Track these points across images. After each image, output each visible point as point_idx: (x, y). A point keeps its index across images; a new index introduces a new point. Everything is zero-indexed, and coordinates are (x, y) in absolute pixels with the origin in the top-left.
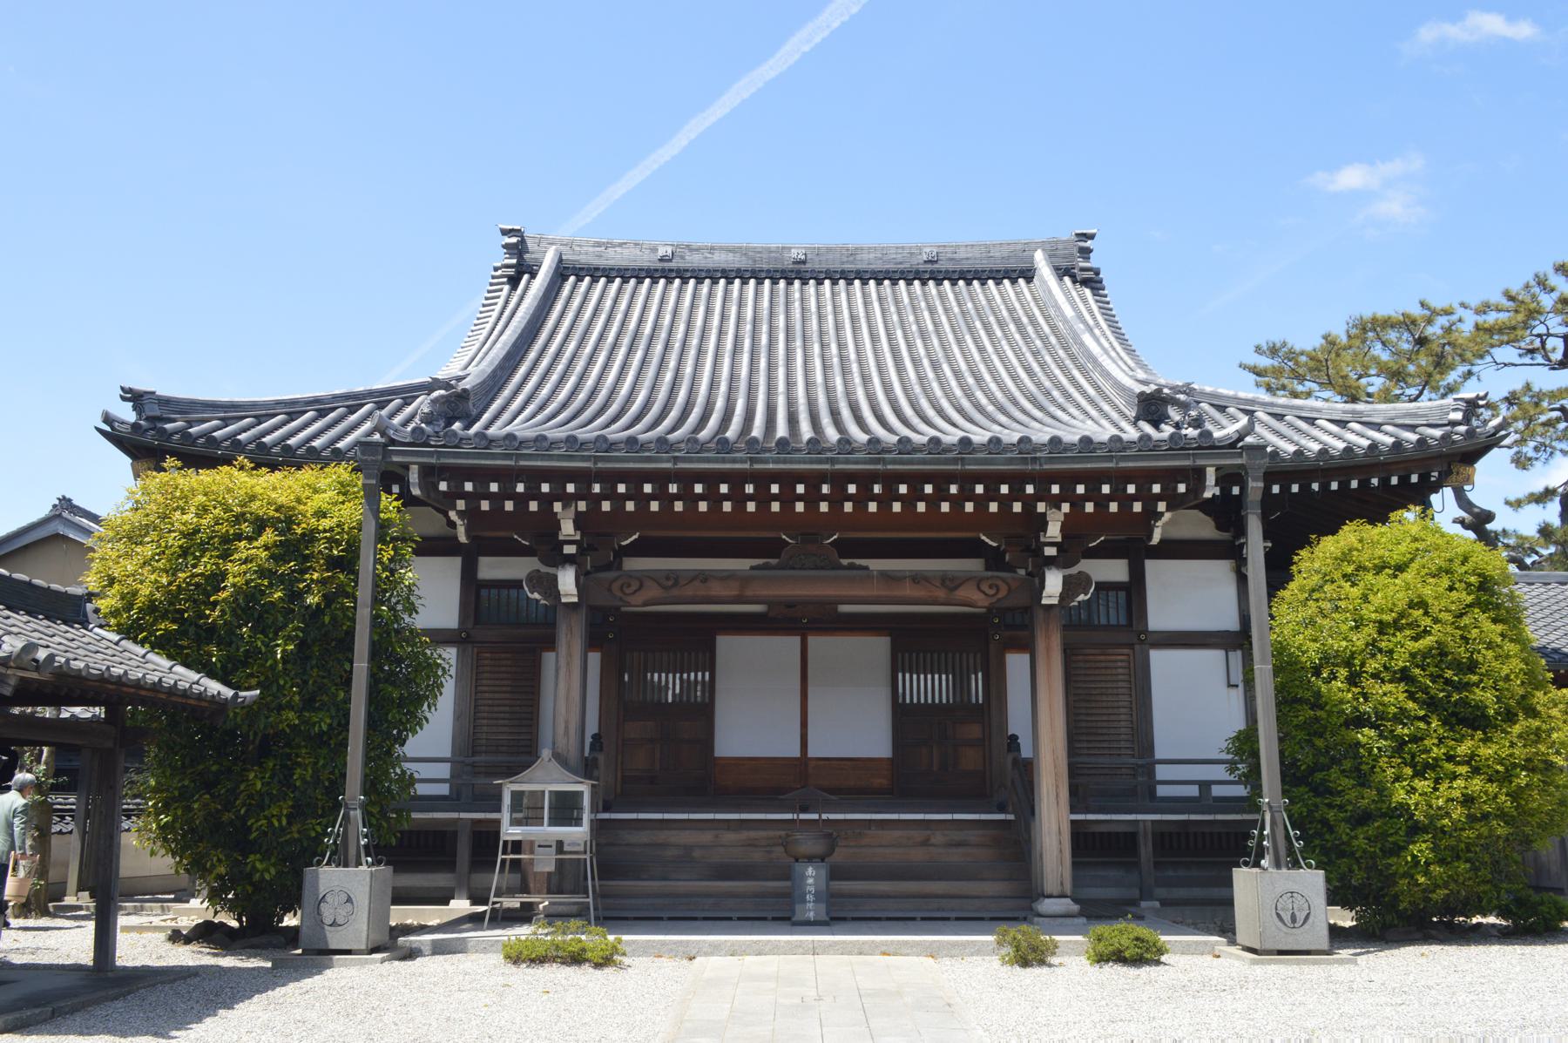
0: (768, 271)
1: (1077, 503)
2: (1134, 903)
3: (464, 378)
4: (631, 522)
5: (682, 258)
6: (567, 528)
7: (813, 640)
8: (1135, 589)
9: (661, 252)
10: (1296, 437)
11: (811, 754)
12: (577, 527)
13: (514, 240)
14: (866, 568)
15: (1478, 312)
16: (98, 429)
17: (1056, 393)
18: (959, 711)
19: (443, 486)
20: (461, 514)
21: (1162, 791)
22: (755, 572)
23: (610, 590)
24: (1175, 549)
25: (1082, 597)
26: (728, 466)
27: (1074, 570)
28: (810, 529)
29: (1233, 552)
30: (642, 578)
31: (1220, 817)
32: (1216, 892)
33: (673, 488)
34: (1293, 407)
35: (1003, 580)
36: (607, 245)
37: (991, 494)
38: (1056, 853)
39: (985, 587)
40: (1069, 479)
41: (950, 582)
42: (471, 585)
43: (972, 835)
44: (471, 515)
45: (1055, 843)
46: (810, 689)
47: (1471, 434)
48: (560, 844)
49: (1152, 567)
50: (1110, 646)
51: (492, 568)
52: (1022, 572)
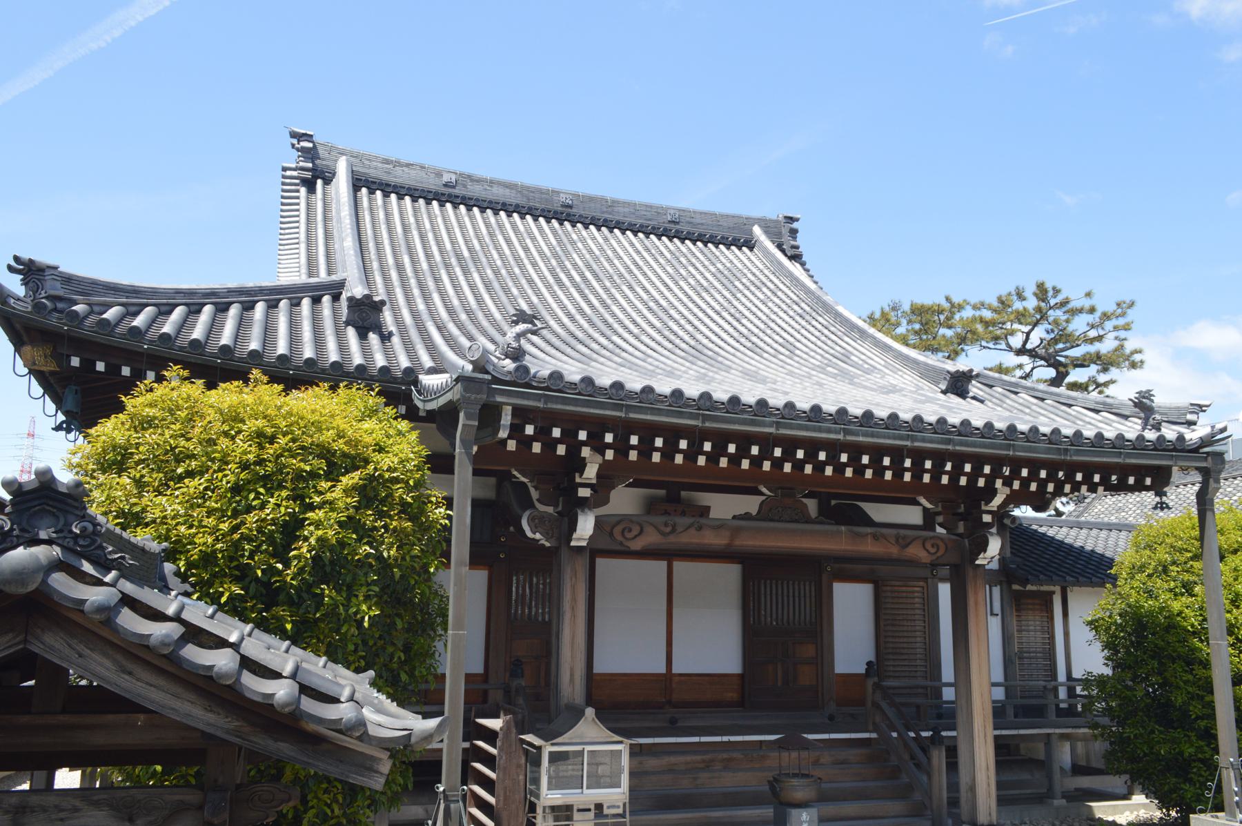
0: (543, 210)
5: (465, 186)
9: (446, 178)
11: (675, 671)
15: (975, 307)
23: (611, 534)
26: (824, 435)
34: (1051, 394)
36: (398, 164)
38: (985, 786)
39: (928, 546)
43: (853, 754)
45: (984, 778)
46: (675, 611)
48: (599, 807)
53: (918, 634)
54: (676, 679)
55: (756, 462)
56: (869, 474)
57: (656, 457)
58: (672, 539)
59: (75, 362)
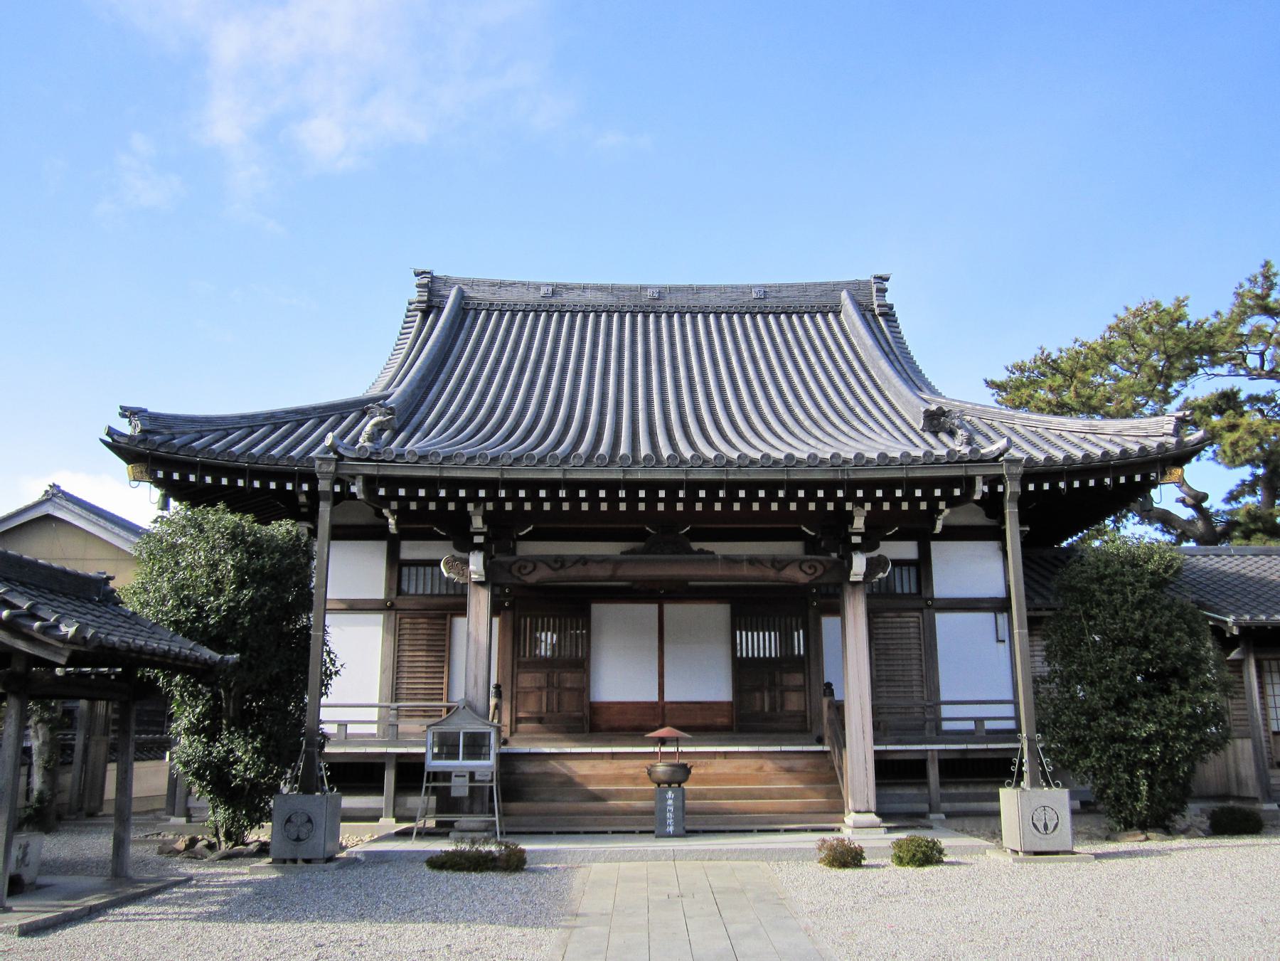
1: (877, 503)
2: (923, 815)
3: (389, 396)
4: (525, 518)
6: (477, 523)
7: (669, 608)
8: (922, 566)
10: (1046, 447)
12: (484, 522)
13: (425, 281)
14: (712, 553)
16: (102, 441)
17: (858, 410)
18: (787, 662)
19: (382, 492)
20: (393, 512)
21: (946, 726)
22: (624, 557)
23: (510, 571)
24: (953, 533)
25: (881, 575)
27: (874, 554)
28: (669, 523)
29: (997, 534)
30: (536, 561)
31: (991, 746)
32: (987, 806)
33: (522, 494)
35: (821, 562)
36: (501, 285)
37: (811, 496)
39: (805, 567)
40: (870, 485)
41: (779, 563)
42: (396, 564)
44: (402, 514)
47: (1179, 443)
48: (472, 775)
49: (935, 546)
50: (905, 608)
51: (410, 551)
52: (834, 555)
53: (914, 662)
54: (668, 707)
55: (802, 503)
56: (547, 506)
57: (642, 507)
58: (562, 573)
59: (257, 484)
